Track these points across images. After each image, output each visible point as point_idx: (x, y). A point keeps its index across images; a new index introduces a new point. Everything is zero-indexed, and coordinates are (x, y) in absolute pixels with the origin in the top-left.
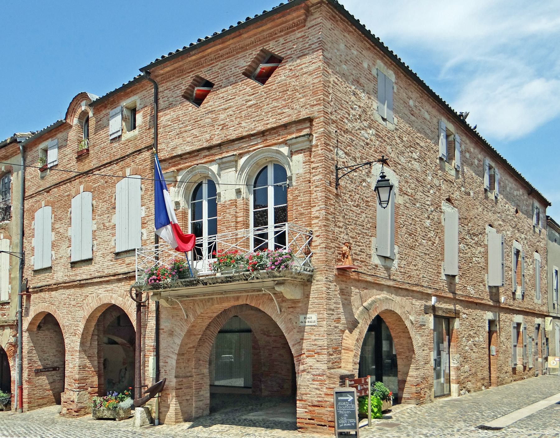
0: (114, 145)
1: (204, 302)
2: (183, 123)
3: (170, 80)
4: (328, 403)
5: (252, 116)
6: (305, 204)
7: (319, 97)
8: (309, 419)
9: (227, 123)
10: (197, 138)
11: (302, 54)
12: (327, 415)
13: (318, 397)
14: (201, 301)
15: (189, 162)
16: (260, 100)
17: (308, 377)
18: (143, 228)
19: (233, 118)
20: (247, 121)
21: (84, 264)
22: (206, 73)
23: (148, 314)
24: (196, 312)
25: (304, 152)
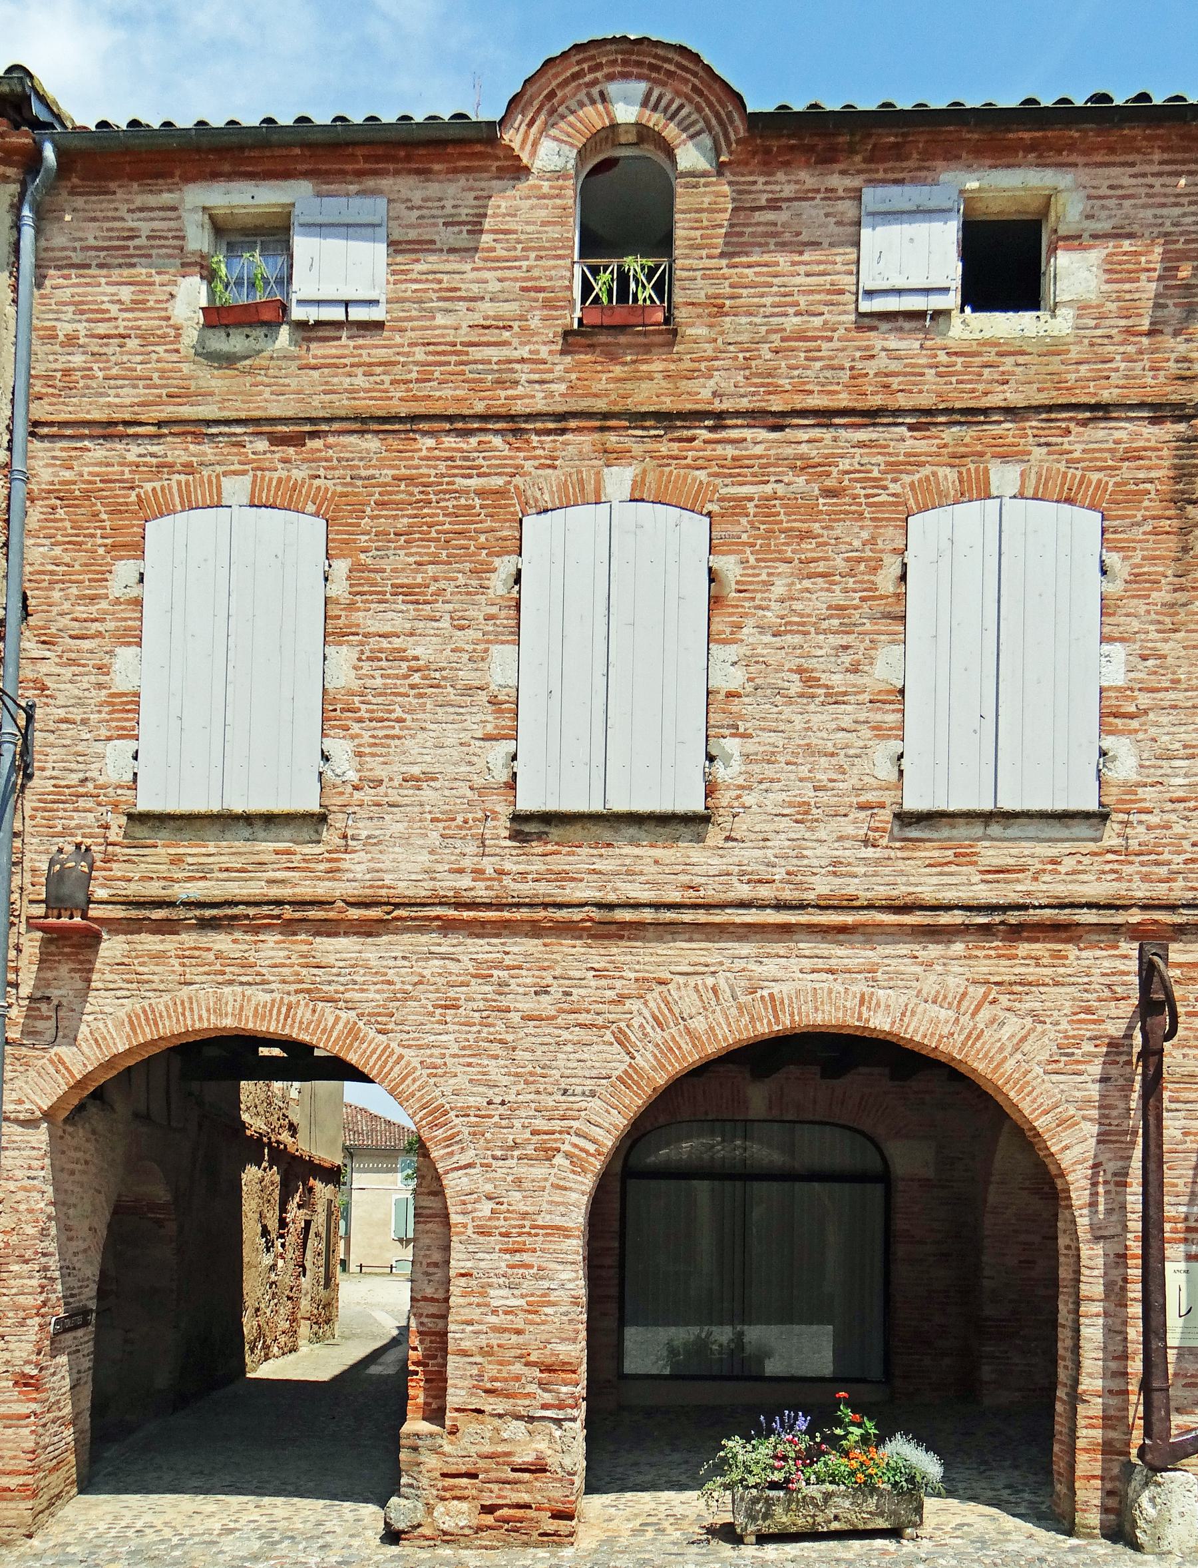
0: (893, 343)
21: (632, 831)
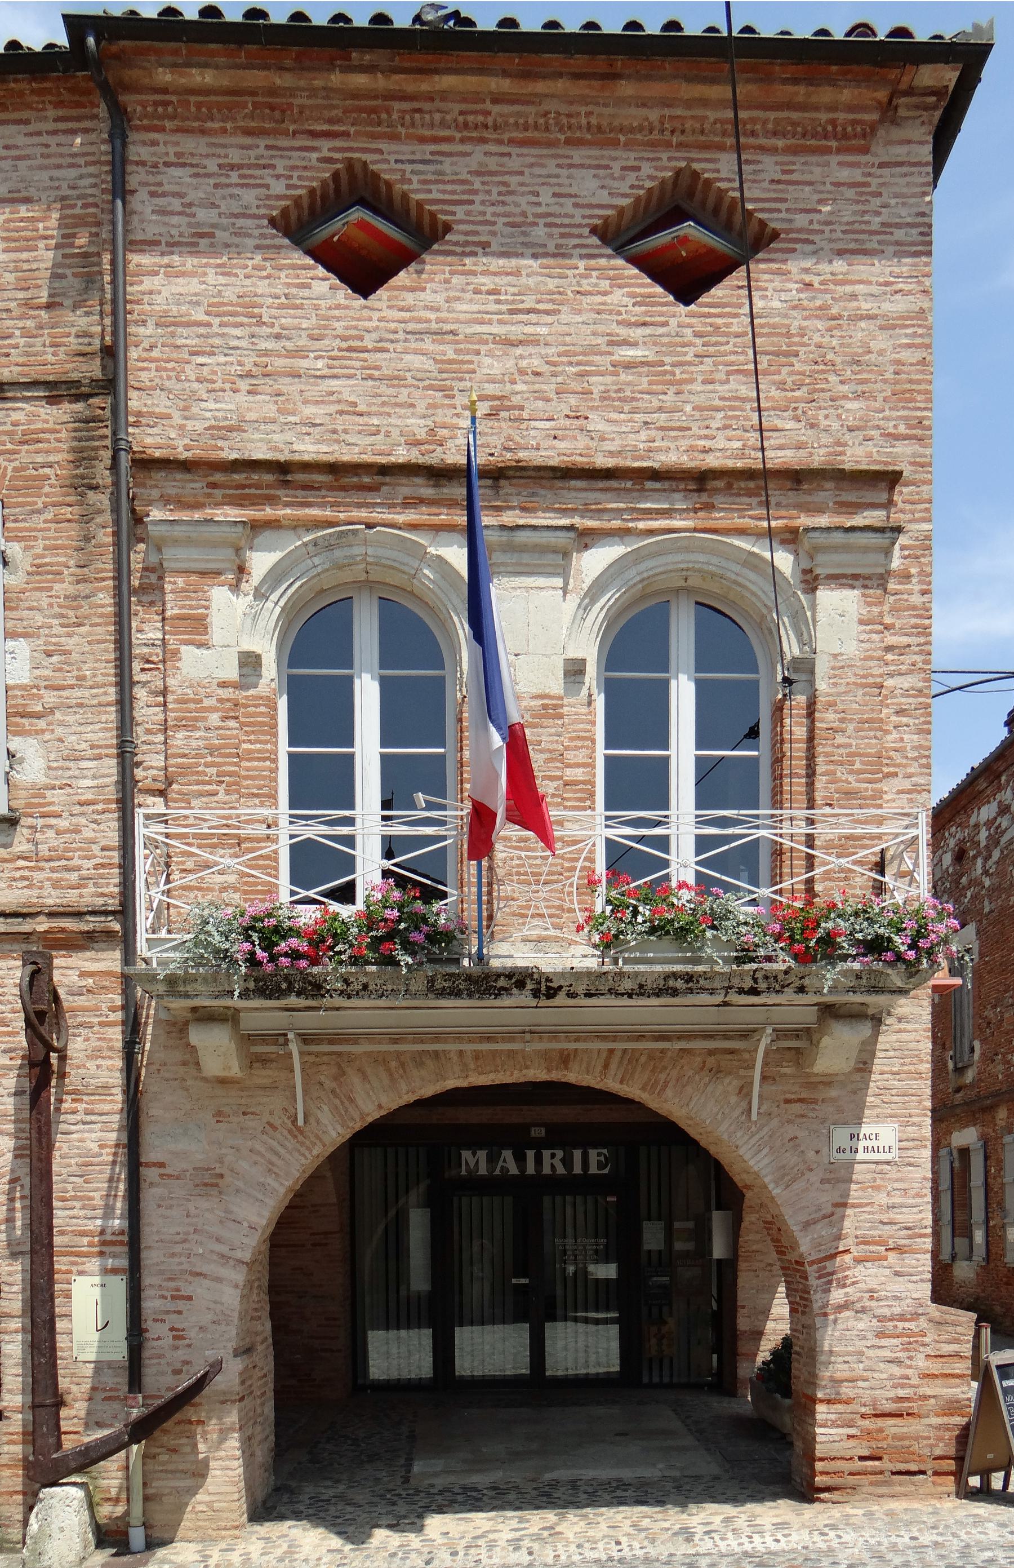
1: (393, 1064)
2: (278, 337)
3: (203, 132)
4: (933, 1401)
5: (640, 404)
6: (862, 763)
7: (919, 414)
8: (862, 1458)
9: (516, 400)
10: (357, 419)
11: (852, 246)
12: (929, 1438)
13: (895, 1387)
14: (380, 1060)
15: (322, 505)
16: (678, 354)
17: (861, 1325)
18: (13, 730)
19: (549, 388)
20: (614, 416)
22: (408, 168)
23: (60, 1101)
24: (352, 1100)
25: (865, 587)
